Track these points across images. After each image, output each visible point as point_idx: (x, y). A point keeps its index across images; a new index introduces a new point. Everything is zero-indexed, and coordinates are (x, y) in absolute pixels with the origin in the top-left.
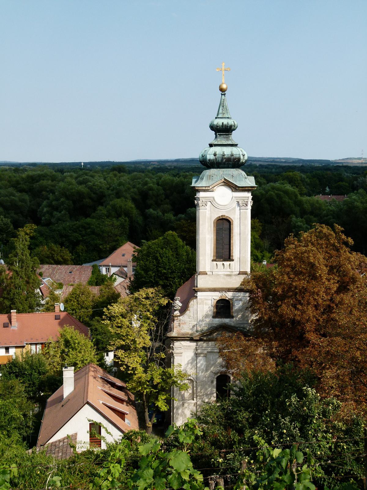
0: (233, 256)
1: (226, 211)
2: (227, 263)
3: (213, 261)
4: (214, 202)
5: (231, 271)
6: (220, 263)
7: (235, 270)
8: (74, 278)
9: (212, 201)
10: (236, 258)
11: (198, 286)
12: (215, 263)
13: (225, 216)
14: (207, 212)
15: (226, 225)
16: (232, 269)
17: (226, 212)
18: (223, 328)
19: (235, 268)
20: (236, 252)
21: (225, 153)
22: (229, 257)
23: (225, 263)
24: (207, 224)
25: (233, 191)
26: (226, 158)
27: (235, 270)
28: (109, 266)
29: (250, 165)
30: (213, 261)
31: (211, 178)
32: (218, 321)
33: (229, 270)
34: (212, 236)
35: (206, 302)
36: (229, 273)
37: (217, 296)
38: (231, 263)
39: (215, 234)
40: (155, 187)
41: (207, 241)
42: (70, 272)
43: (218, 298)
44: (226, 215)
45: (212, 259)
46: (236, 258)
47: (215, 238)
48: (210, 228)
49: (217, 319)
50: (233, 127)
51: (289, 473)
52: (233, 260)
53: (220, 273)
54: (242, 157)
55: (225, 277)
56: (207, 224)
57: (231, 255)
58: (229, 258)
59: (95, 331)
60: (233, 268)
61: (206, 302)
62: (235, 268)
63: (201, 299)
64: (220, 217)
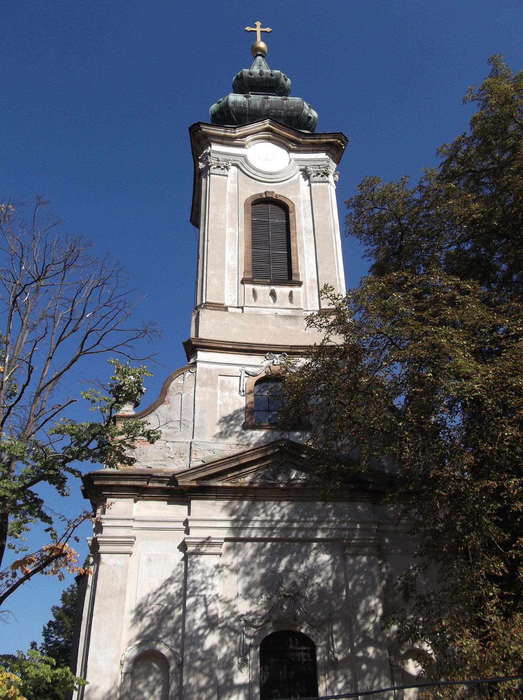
0: (298, 275)
2: (282, 291)
3: (243, 282)
4: (246, 165)
5: (293, 306)
6: (264, 290)
7: (307, 307)
9: (242, 166)
12: (249, 287)
13: (273, 192)
14: (229, 184)
15: (276, 218)
16: (299, 304)
20: (306, 265)
22: (289, 277)
23: (278, 290)
24: (228, 206)
25: (290, 150)
28: (110, 417)
30: (243, 282)
33: (289, 305)
34: (242, 230)
35: (222, 382)
36: (289, 312)
37: (259, 365)
38: (295, 289)
39: (250, 227)
41: (228, 239)
45: (241, 277)
47: (250, 233)
48: (235, 215)
51: (271, 478)
52: (299, 284)
53: (264, 311)
55: (280, 321)
56: (228, 206)
57: (294, 271)
59: (257, 555)
60: (302, 301)
61: (222, 382)
62: (306, 302)
63: (208, 372)
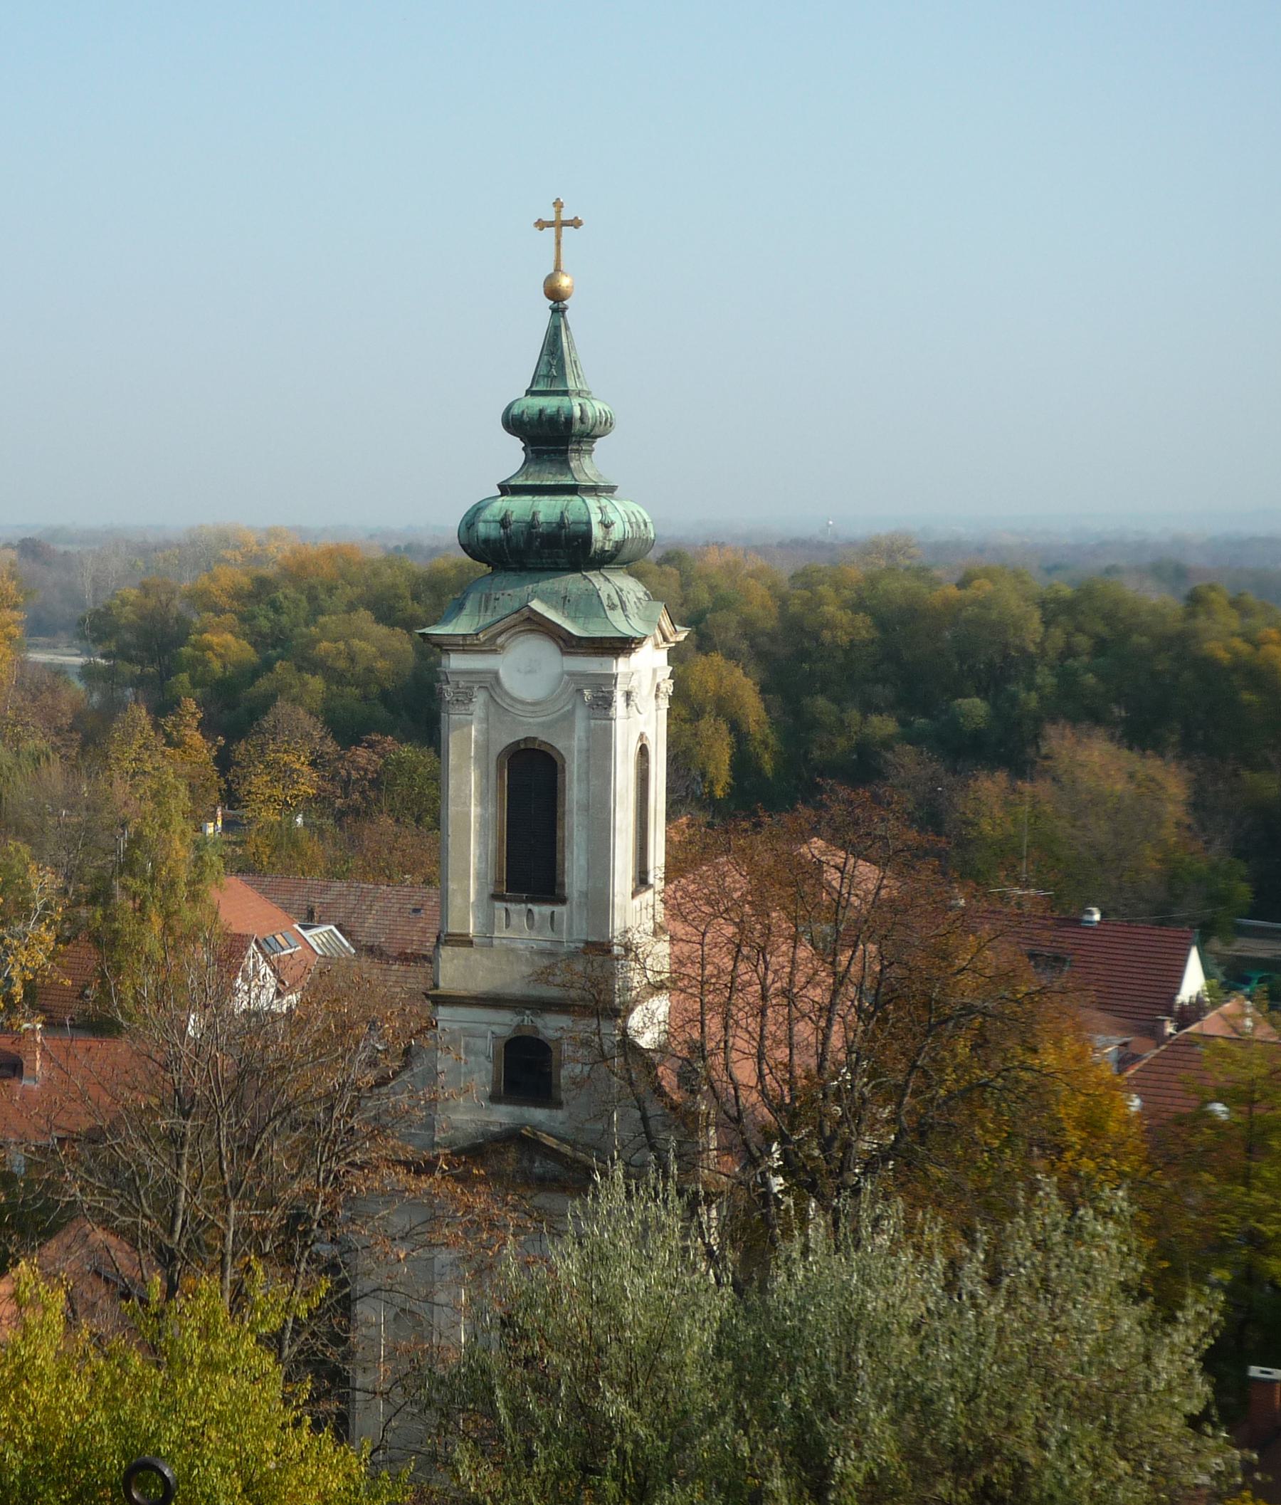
1: (539, 724)
5: (555, 938)
8: (424, 931)
9: (492, 683)
10: (576, 895)
11: (441, 984)
13: (535, 739)
16: (561, 932)
17: (542, 725)
18: (515, 1138)
19: (570, 928)
21: (541, 518)
26: (541, 536)
27: (570, 933)
29: (673, 558)
31: (491, 607)
32: (503, 1116)
33: (549, 935)
38: (558, 909)
40: (843, 617)
42: (416, 911)
43: (506, 1032)
44: (543, 737)
46: (576, 895)
49: (503, 1108)
50: (577, 427)
52: (562, 900)
54: (597, 532)
58: (553, 893)
64: (518, 742)
